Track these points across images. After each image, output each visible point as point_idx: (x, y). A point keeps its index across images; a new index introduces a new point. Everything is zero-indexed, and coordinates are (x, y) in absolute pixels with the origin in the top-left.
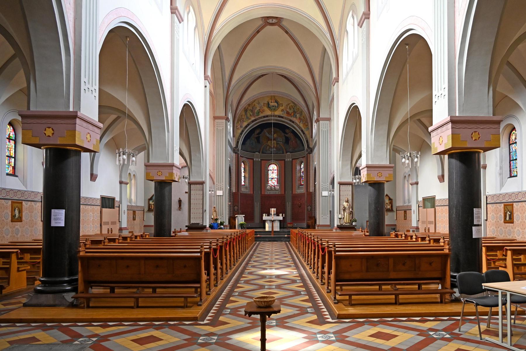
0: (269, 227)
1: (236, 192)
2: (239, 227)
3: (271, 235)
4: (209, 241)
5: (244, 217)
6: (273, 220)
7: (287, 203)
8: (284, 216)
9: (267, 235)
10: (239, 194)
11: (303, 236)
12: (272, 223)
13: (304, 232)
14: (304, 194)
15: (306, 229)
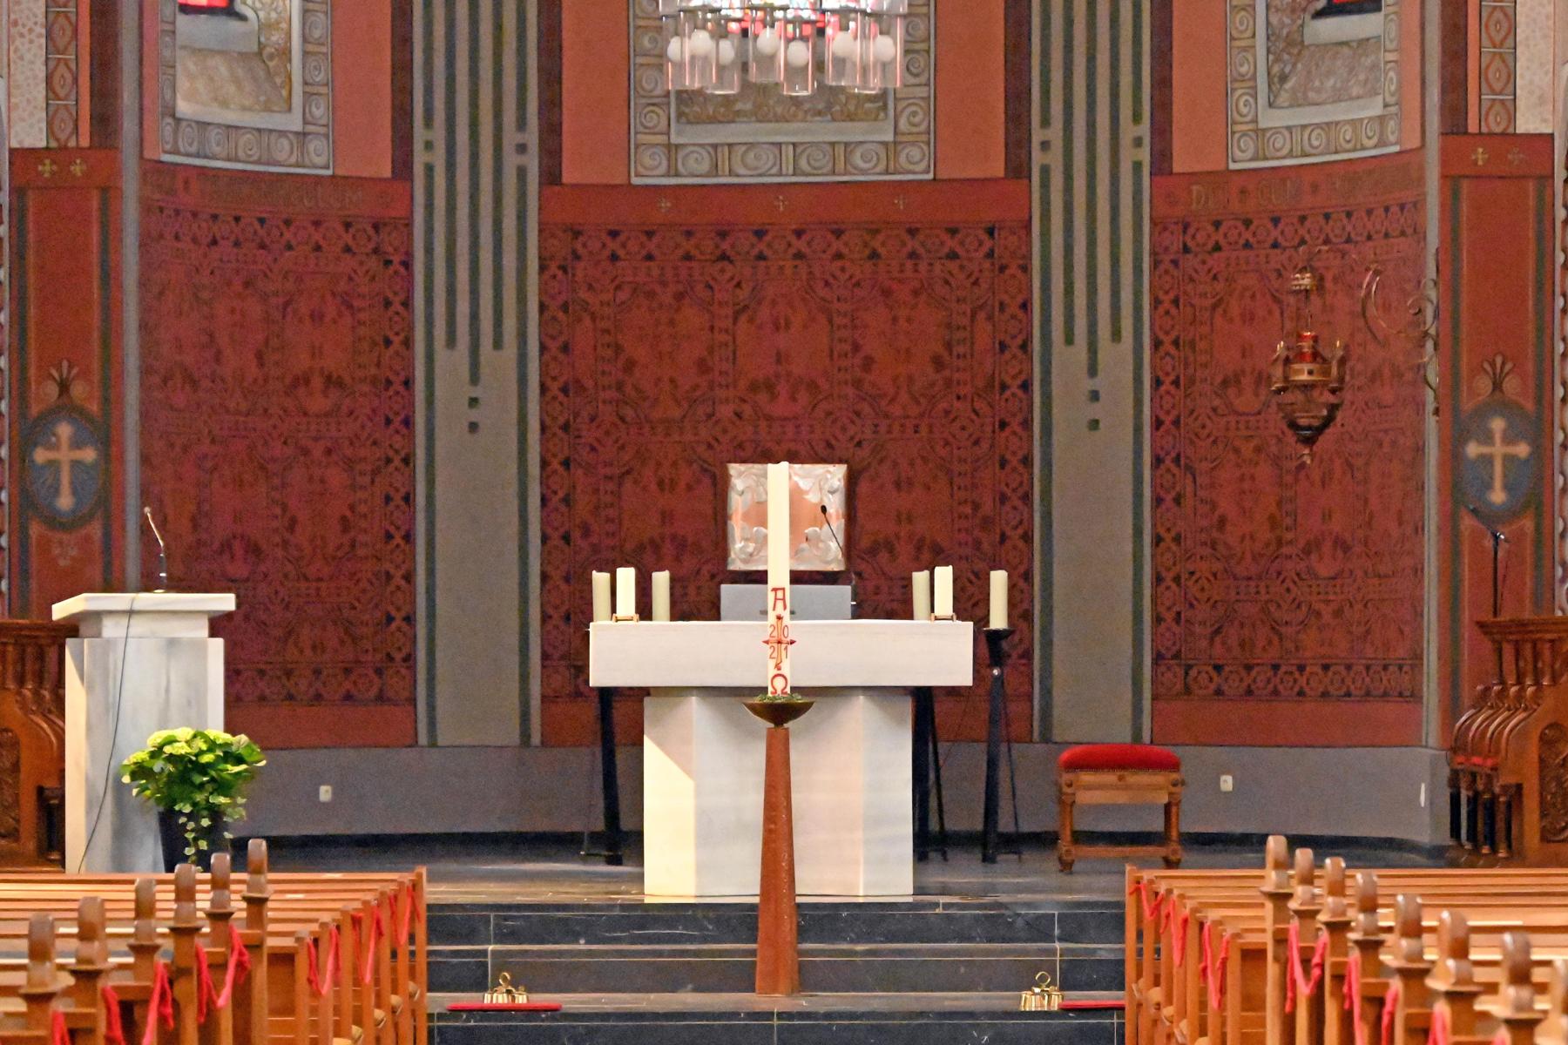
0: (708, 832)
1: (57, 153)
2: (121, 833)
3: (743, 978)
4: (315, 921)
5: (218, 625)
6: (778, 689)
7: (1068, 360)
8: (998, 620)
9: (668, 979)
10: (130, 186)
11: (1376, 1002)
12: (756, 757)
13: (1385, 918)
14: (1404, 166)
15: (1437, 856)
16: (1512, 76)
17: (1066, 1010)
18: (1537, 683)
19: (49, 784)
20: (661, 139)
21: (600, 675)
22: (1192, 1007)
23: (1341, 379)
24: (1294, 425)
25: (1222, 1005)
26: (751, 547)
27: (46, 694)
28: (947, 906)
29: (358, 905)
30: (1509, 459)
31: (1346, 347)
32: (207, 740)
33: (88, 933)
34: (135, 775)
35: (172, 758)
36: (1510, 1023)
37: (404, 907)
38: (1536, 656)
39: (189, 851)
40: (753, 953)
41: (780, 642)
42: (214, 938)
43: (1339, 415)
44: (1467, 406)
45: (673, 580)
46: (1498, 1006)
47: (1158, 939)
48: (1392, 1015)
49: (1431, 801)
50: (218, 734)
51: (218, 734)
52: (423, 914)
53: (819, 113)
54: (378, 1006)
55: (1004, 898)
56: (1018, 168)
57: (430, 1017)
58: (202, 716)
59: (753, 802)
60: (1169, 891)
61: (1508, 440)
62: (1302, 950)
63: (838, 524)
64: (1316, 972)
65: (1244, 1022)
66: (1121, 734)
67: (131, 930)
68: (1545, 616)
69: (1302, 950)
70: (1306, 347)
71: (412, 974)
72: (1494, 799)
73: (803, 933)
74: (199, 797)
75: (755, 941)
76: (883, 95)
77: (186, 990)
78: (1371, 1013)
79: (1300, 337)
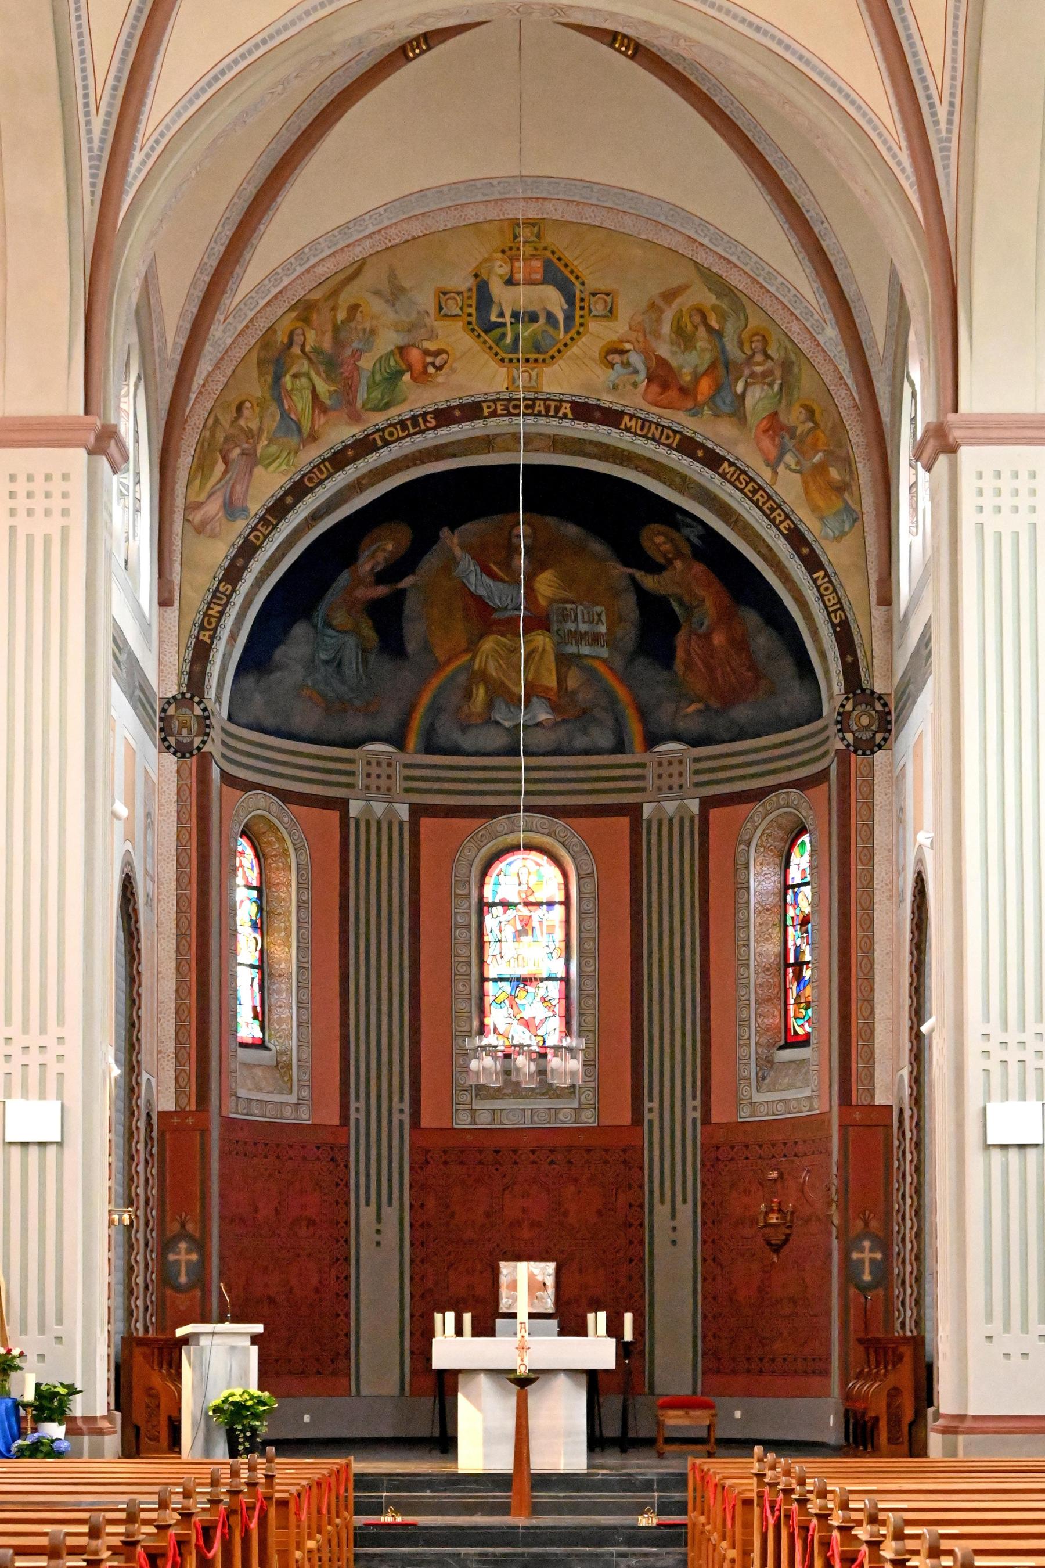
0: (489, 1438)
3: (504, 1509)
4: (299, 1484)
5: (255, 1339)
6: (522, 1371)
7: (661, 1211)
8: (628, 1336)
9: (469, 1509)
11: (805, 1528)
12: (513, 1401)
14: (819, 1121)
16: (872, 1076)
17: (659, 1526)
18: (886, 1367)
19: (174, 1414)
20: (469, 1107)
21: (437, 1364)
22: (719, 1526)
23: (792, 1221)
24: (769, 1243)
25: (733, 1525)
26: (510, 1301)
27: (173, 1371)
28: (603, 1475)
29: (319, 1476)
30: (872, 1261)
31: (794, 1207)
32: (249, 1394)
33: (187, 1495)
34: (215, 1411)
35: (233, 1403)
36: (867, 1542)
37: (343, 1476)
38: (886, 1354)
39: (241, 1448)
40: (509, 1497)
41: (523, 1348)
42: (249, 1495)
43: (791, 1238)
44: (852, 1234)
45: (473, 1317)
46: (863, 1533)
47: (703, 1491)
48: (813, 1536)
49: (835, 1422)
50: (257, 1393)
51: (254, 1390)
52: (352, 1478)
53: (543, 1094)
54: (329, 1524)
55: (629, 1471)
56: (638, 1119)
57: (355, 1528)
58: (247, 1384)
59: (511, 1424)
60: (709, 1470)
61: (871, 1251)
62: (770, 1502)
63: (551, 1290)
64: (777, 1513)
65: (743, 1534)
66: (686, 1390)
67: (209, 1490)
68: (890, 1336)
69: (770, 1502)
70: (775, 1207)
71: (347, 1509)
72: (865, 1423)
73: (533, 1488)
74: (245, 1422)
75: (510, 1491)
76: (573, 1086)
77: (236, 1521)
78: (803, 1534)
79: (773, 1202)
